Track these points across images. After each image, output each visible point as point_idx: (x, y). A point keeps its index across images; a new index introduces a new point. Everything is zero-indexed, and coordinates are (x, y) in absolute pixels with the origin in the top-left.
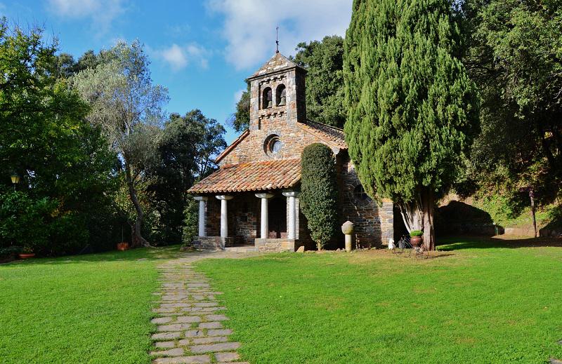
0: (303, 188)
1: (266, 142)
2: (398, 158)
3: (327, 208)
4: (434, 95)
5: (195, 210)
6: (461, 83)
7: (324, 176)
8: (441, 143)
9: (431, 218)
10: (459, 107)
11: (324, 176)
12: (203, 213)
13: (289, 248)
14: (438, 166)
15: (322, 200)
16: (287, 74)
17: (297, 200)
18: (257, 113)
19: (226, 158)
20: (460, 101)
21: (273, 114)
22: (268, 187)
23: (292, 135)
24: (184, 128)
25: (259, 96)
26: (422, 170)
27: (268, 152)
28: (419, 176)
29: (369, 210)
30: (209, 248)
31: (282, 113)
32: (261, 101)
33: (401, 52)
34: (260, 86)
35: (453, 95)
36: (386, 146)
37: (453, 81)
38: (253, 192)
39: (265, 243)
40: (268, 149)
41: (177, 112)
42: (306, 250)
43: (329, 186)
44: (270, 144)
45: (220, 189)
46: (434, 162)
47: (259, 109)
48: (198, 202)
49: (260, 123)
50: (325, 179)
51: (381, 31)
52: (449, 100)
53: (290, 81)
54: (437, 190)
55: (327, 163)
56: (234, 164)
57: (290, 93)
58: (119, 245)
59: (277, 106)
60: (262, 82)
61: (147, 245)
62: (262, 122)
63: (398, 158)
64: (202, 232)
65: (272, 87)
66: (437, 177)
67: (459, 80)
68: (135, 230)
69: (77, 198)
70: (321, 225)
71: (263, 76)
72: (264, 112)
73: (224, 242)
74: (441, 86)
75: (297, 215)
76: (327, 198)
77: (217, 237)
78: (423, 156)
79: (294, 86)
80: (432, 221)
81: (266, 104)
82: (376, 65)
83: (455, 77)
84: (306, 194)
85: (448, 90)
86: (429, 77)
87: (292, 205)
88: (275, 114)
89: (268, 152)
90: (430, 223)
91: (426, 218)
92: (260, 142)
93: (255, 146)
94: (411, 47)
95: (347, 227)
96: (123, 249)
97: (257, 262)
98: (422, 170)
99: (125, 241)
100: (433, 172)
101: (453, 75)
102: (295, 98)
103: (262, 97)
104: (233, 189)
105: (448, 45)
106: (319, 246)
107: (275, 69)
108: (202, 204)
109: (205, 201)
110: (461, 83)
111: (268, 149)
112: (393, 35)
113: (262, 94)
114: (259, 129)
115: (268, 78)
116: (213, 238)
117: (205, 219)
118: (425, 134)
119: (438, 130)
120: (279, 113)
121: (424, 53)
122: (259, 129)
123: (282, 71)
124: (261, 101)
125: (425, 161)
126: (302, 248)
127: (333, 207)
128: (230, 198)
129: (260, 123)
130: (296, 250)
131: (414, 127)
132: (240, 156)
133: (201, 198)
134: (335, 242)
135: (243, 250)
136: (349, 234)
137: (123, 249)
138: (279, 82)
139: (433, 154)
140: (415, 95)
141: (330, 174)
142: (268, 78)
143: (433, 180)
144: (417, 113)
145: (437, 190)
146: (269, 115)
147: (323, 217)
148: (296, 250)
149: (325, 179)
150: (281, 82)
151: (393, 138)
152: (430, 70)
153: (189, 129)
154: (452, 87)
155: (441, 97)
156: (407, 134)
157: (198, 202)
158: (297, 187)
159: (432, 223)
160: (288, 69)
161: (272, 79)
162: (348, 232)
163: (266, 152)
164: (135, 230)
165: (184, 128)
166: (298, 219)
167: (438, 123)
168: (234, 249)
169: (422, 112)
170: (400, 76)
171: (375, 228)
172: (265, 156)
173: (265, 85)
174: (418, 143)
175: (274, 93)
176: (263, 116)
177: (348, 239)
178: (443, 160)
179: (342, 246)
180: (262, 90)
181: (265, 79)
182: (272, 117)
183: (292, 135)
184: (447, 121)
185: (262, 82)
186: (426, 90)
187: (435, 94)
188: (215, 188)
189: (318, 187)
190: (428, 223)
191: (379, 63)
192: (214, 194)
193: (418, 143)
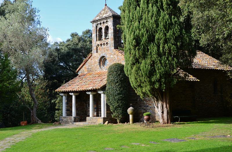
0: (107, 89)
1: (100, 60)
2: (140, 74)
3: (119, 100)
4: (158, 39)
5: (61, 101)
6: (173, 30)
7: (118, 82)
8: (162, 66)
9: (168, 106)
10: (173, 44)
12: (65, 103)
13: (101, 122)
14: (161, 77)
15: (116, 96)
16: (109, 20)
17: (105, 95)
18: (96, 43)
19: (81, 70)
20: (172, 41)
21: (102, 44)
22: (90, 89)
23: (112, 56)
24: (77, 44)
25: (96, 33)
26: (153, 80)
27: (102, 66)
28: (152, 83)
30: (67, 122)
31: (107, 43)
32: (98, 35)
33: (142, 16)
34: (97, 27)
35: (168, 39)
36: (134, 68)
37: (168, 31)
38: (85, 91)
39: (92, 120)
40: (102, 64)
41: (71, 32)
42: (108, 123)
43: (120, 88)
44: (103, 61)
45: (71, 89)
46: (158, 76)
47: (97, 41)
48: (62, 96)
49: (97, 49)
50: (117, 84)
51: (133, 4)
52: (166, 41)
53: (110, 24)
54: (164, 90)
55: (119, 75)
56: (85, 73)
57: (111, 31)
58: (21, 123)
59: (105, 39)
60: (98, 24)
61: (40, 122)
62: (98, 49)
63: (140, 74)
64: (64, 114)
65: (102, 27)
66: (162, 83)
67: (172, 29)
68: (33, 113)
69: (206, 49)
70: (116, 109)
71: (97, 21)
72: (99, 42)
73: (73, 119)
74: (161, 34)
75: (106, 104)
76: (119, 94)
77: (70, 117)
78: (151, 73)
79: (112, 27)
80: (168, 107)
81: (100, 39)
82: (130, 24)
83: (170, 28)
84: (108, 92)
85: (166, 35)
86: (155, 29)
87: (103, 98)
88: (104, 44)
89: (102, 66)
90: (167, 108)
91: (165, 106)
92: (97, 60)
93: (95, 63)
94: (146, 13)
95: (130, 110)
96: (23, 125)
97: (82, 129)
98: (153, 80)
99: (25, 120)
100: (159, 81)
101: (168, 27)
102: (113, 35)
103: (98, 33)
104: (75, 90)
105: (168, 9)
106: (118, 121)
107: (103, 16)
108: (64, 97)
109: (65, 96)
110: (173, 30)
111: (102, 64)
112: (139, 5)
113: (98, 32)
115: (100, 22)
116: (69, 117)
117: (66, 106)
118: (152, 61)
119: (159, 58)
120: (105, 43)
121: (152, 16)
123: (106, 18)
124: (98, 35)
125: (153, 75)
127: (122, 99)
128: (77, 94)
129: (97, 49)
130: (104, 123)
131: (147, 57)
132: (88, 69)
133: (72, 94)
134: (125, 120)
135: (81, 124)
136: (131, 114)
137: (23, 125)
138: (106, 25)
139: (157, 71)
140: (146, 40)
141: (121, 81)
142: (100, 22)
143: (160, 85)
144: (148, 49)
145: (164, 90)
146: (101, 45)
147: (116, 105)
148: (104, 123)
149: (117, 84)
150: (107, 25)
151: (137, 63)
152: (155, 26)
153: (80, 45)
154: (168, 34)
155: (161, 40)
156: (143, 62)
157: (62, 96)
158: (103, 88)
159: (168, 108)
160: (109, 17)
161: (102, 22)
162: (130, 113)
163: (100, 66)
164: (33, 113)
165: (77, 44)
166: (106, 106)
167: (159, 55)
168: (77, 123)
169: (151, 49)
170: (140, 30)
171: (153, 111)
173: (99, 26)
174: (148, 66)
175: (103, 31)
176: (98, 45)
177: (131, 117)
178: (163, 74)
179: (128, 121)
180: (98, 29)
181: (99, 23)
182: (103, 46)
183: (112, 56)
184: (165, 53)
185: (98, 24)
186: (154, 37)
187: (158, 38)
189: (114, 88)
190: (166, 108)
191: (131, 22)
192: (69, 92)
193: (148, 66)
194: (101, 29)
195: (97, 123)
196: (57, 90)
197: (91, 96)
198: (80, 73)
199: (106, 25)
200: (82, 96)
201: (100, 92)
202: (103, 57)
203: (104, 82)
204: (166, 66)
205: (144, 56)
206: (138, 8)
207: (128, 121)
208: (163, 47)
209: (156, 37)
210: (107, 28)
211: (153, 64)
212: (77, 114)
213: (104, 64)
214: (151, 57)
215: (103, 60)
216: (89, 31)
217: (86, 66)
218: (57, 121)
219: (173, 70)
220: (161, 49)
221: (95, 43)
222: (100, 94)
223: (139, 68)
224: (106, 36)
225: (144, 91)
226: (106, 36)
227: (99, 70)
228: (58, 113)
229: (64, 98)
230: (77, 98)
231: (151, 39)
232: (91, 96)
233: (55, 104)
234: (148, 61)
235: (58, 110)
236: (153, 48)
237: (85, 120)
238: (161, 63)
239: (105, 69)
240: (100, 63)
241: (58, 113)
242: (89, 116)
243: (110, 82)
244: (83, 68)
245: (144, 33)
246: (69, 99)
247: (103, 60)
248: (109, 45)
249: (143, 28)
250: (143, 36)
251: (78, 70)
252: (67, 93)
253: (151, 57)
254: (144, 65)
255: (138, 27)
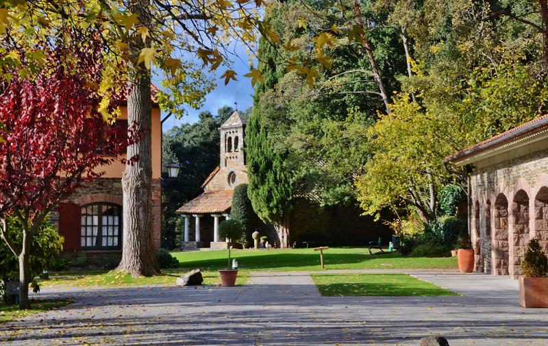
1: (229, 176)
5: (183, 223)
7: (243, 205)
11: (243, 205)
14: (277, 202)
16: (238, 130)
24: (208, 135)
27: (231, 183)
28: (270, 209)
29: (446, 223)
46: (275, 202)
48: (184, 218)
64: (186, 239)
72: (228, 154)
76: (243, 218)
78: (269, 199)
89: (231, 183)
92: (226, 176)
95: (254, 234)
100: (276, 207)
106: (244, 246)
112: (259, 131)
114: (226, 166)
122: (226, 166)
126: (231, 247)
128: (201, 216)
138: (236, 134)
143: (278, 210)
156: (262, 188)
163: (229, 183)
165: (208, 135)
167: (276, 182)
170: (259, 157)
172: (228, 186)
173: (229, 135)
179: (252, 246)
182: (232, 159)
188: (192, 211)
192: (192, 214)
194: (230, 138)
195: (222, 249)
196: (177, 211)
197: (216, 219)
198: (206, 191)
199: (236, 134)
200: (206, 219)
201: (224, 215)
202: (233, 172)
203: (230, 204)
204: (282, 193)
205: (263, 182)
206: (258, 135)
207: (252, 246)
208: (280, 175)
209: (274, 165)
210: (237, 139)
211: (270, 191)
212: (201, 239)
213: (234, 180)
214: (269, 184)
215: (232, 176)
216: (229, 109)
217: (214, 180)
218: (177, 247)
219: (289, 197)
220: (278, 176)
221: (224, 154)
222: (214, 218)
223: (258, 194)
224: (236, 147)
225: (264, 216)
226: (236, 147)
227: (227, 188)
228: (179, 238)
229: (186, 220)
230: (201, 219)
231: (269, 165)
232: (216, 219)
233: (174, 225)
234: (266, 187)
235: (180, 233)
236: (270, 176)
237: (209, 246)
238: (277, 189)
239: (233, 186)
240: (229, 179)
241: (179, 238)
242: (213, 241)
243: (236, 204)
244: (210, 183)
245: (366, 65)
246: (192, 220)
247: (232, 176)
248: (238, 159)
249: (262, 155)
250: (261, 163)
251: (204, 184)
252: (190, 215)
253: (269, 184)
254: (263, 190)
255: (258, 154)
